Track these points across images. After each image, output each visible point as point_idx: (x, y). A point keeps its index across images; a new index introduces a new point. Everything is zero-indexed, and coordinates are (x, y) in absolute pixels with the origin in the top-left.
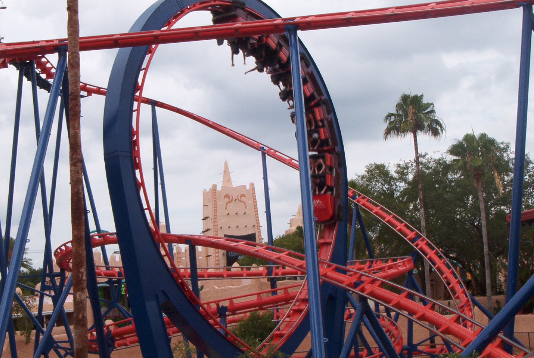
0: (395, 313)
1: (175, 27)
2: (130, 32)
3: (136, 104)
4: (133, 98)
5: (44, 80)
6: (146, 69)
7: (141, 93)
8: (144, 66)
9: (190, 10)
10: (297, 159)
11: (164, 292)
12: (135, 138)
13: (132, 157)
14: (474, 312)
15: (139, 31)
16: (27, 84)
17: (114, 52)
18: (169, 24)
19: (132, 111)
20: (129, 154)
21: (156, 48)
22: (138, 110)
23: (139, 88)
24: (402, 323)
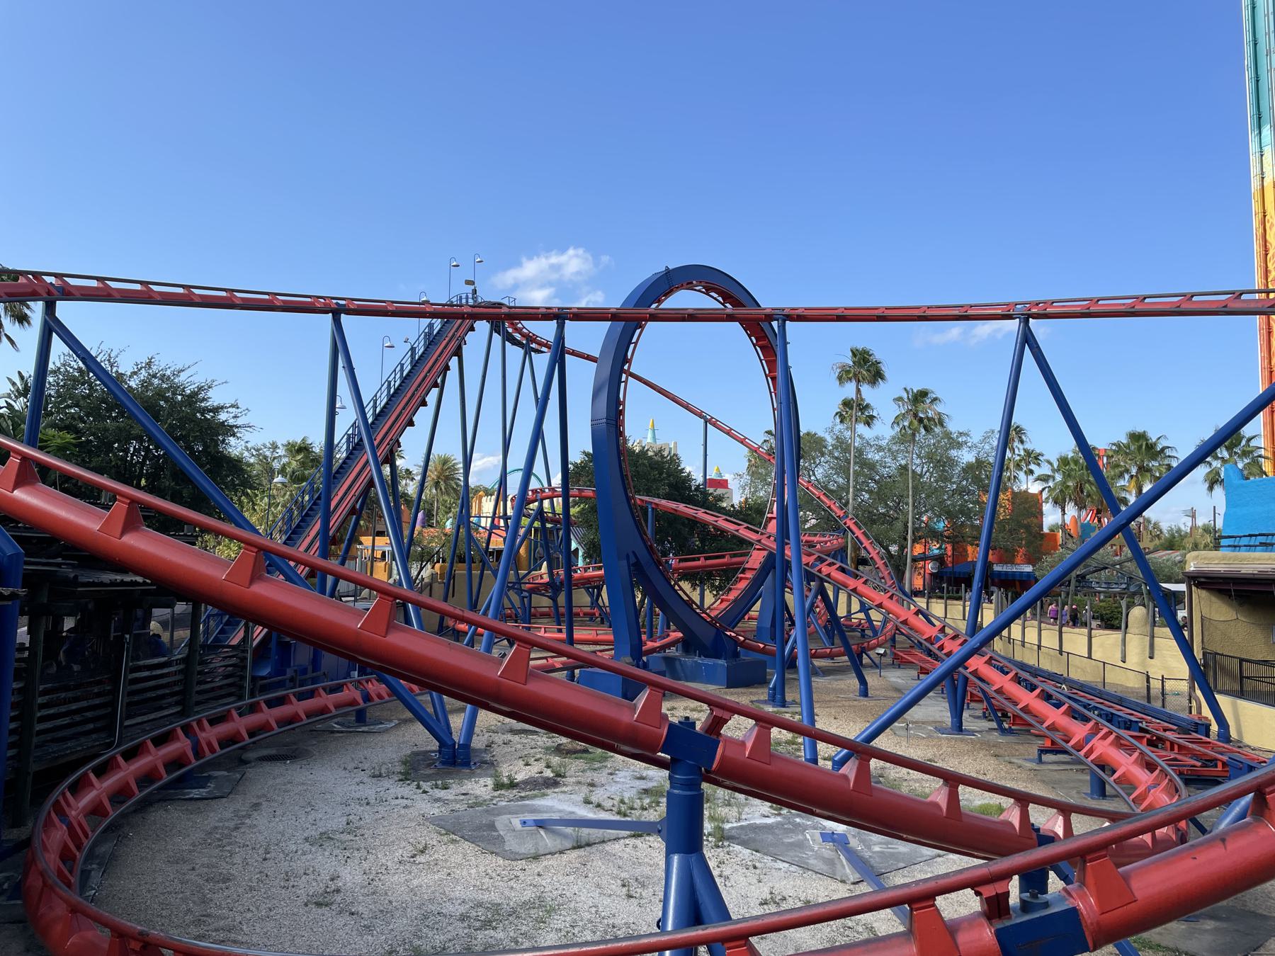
0: (1016, 878)
1: (663, 306)
2: (623, 307)
3: (624, 376)
4: (622, 371)
5: (510, 334)
6: (636, 343)
7: (629, 367)
8: (634, 340)
9: (678, 288)
10: (839, 749)
11: (634, 552)
12: (621, 408)
13: (617, 426)
14: (1000, 655)
15: (631, 307)
16: (497, 338)
17: (606, 325)
18: (659, 301)
19: (620, 382)
20: (614, 423)
21: (645, 324)
22: (626, 382)
23: (626, 360)
24: (843, 597)
